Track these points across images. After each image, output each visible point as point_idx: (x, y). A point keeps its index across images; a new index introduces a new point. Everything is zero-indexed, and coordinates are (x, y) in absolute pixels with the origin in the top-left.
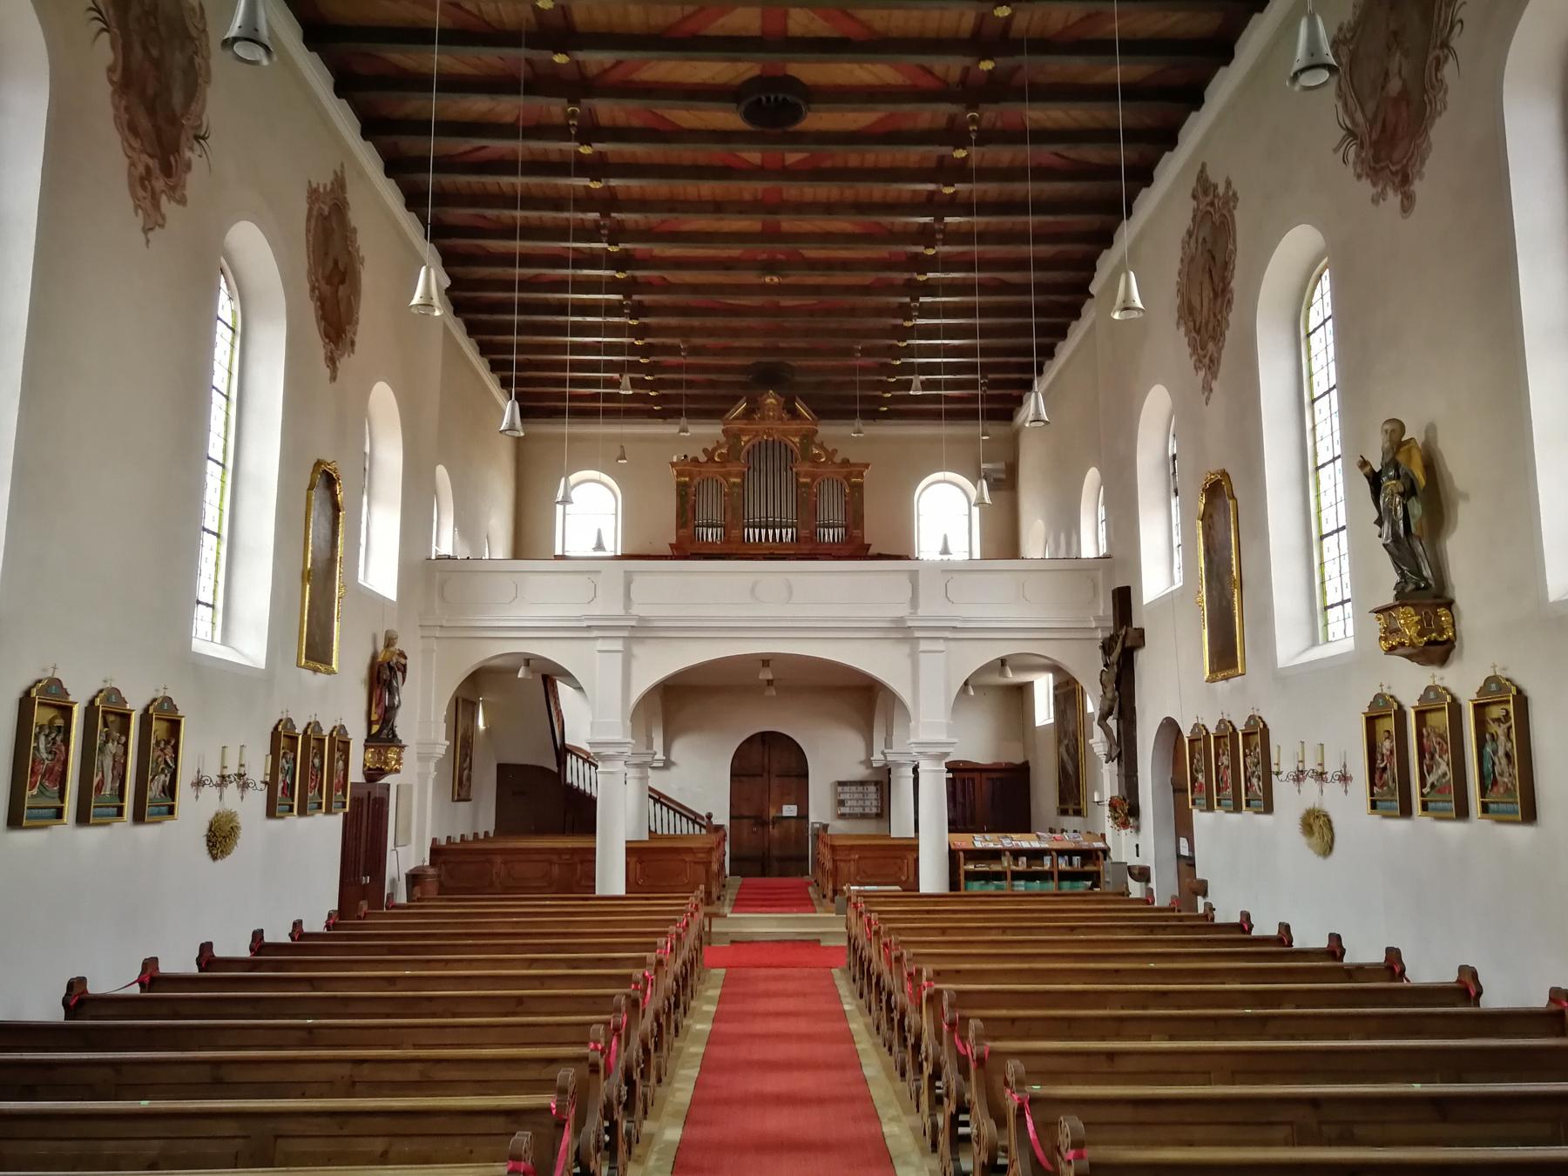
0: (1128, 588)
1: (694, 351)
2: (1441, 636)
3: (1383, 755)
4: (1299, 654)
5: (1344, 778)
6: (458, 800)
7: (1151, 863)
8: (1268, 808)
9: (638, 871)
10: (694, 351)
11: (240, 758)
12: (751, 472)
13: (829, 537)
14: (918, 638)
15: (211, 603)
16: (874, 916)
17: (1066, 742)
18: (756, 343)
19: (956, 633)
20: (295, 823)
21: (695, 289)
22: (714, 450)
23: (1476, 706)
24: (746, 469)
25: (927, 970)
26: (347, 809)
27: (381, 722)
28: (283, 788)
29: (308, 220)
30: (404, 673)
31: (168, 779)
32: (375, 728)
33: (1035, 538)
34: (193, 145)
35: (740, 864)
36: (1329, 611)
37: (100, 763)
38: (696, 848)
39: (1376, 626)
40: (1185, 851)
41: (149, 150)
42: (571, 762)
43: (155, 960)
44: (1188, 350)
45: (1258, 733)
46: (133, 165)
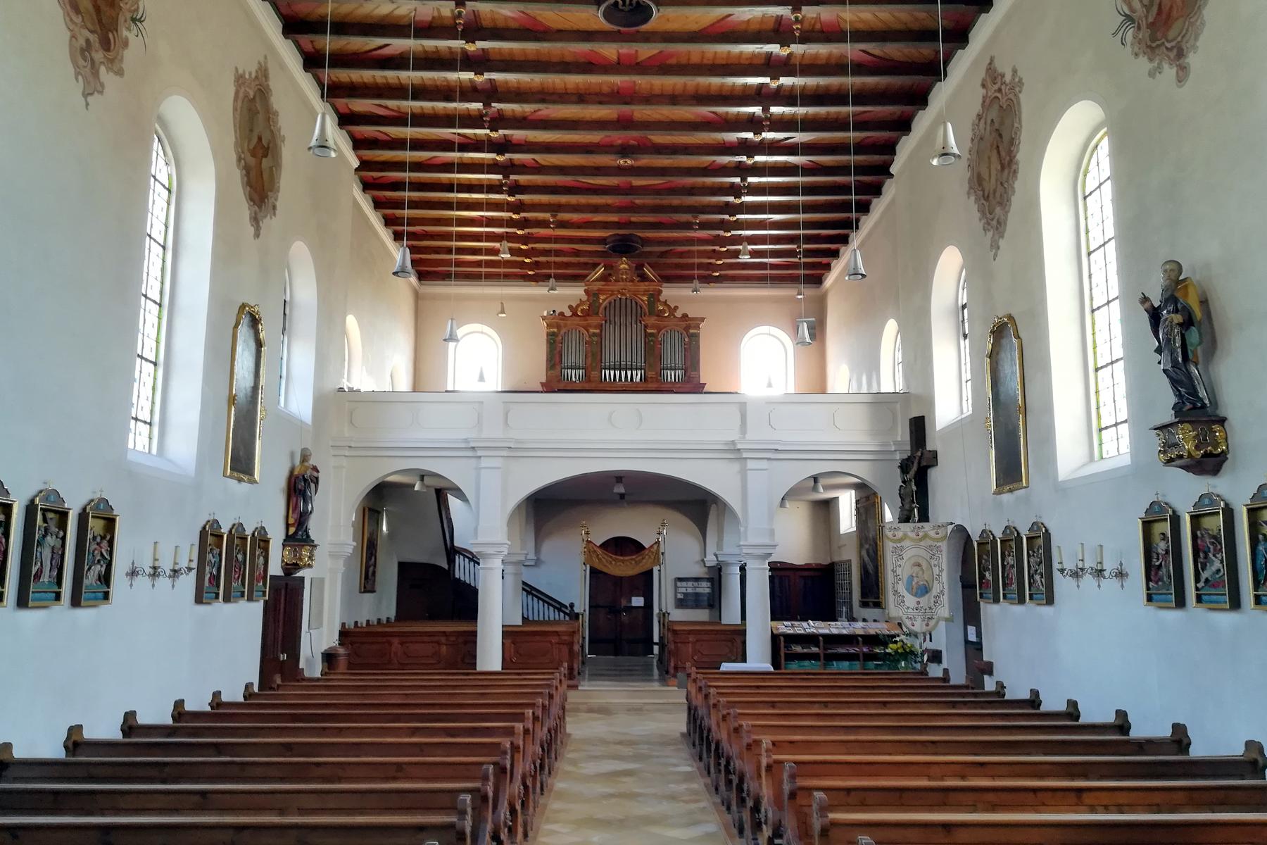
0: (923, 417)
1: (563, 225)
2: (1216, 449)
3: (1158, 554)
4: (1080, 468)
5: (1121, 575)
6: (365, 592)
7: (942, 647)
8: (1050, 601)
9: (512, 651)
10: (563, 225)
11: (155, 554)
12: (608, 325)
13: (671, 378)
14: (746, 458)
15: (149, 421)
16: (712, 691)
17: (867, 546)
18: (613, 218)
19: (774, 453)
20: (220, 609)
21: (562, 170)
22: (578, 306)
23: (1192, 517)
24: (604, 322)
25: (766, 740)
26: (267, 598)
27: (296, 525)
28: (210, 579)
29: (236, 99)
30: (317, 483)
31: (103, 570)
32: (292, 530)
33: (840, 377)
34: (130, 26)
35: (598, 644)
36: (1103, 432)
37: (38, 554)
38: (560, 632)
39: (1156, 442)
40: (972, 637)
41: (89, 25)
42: (459, 560)
43: (80, 727)
44: (978, 215)
45: (1041, 539)
46: (73, 37)
